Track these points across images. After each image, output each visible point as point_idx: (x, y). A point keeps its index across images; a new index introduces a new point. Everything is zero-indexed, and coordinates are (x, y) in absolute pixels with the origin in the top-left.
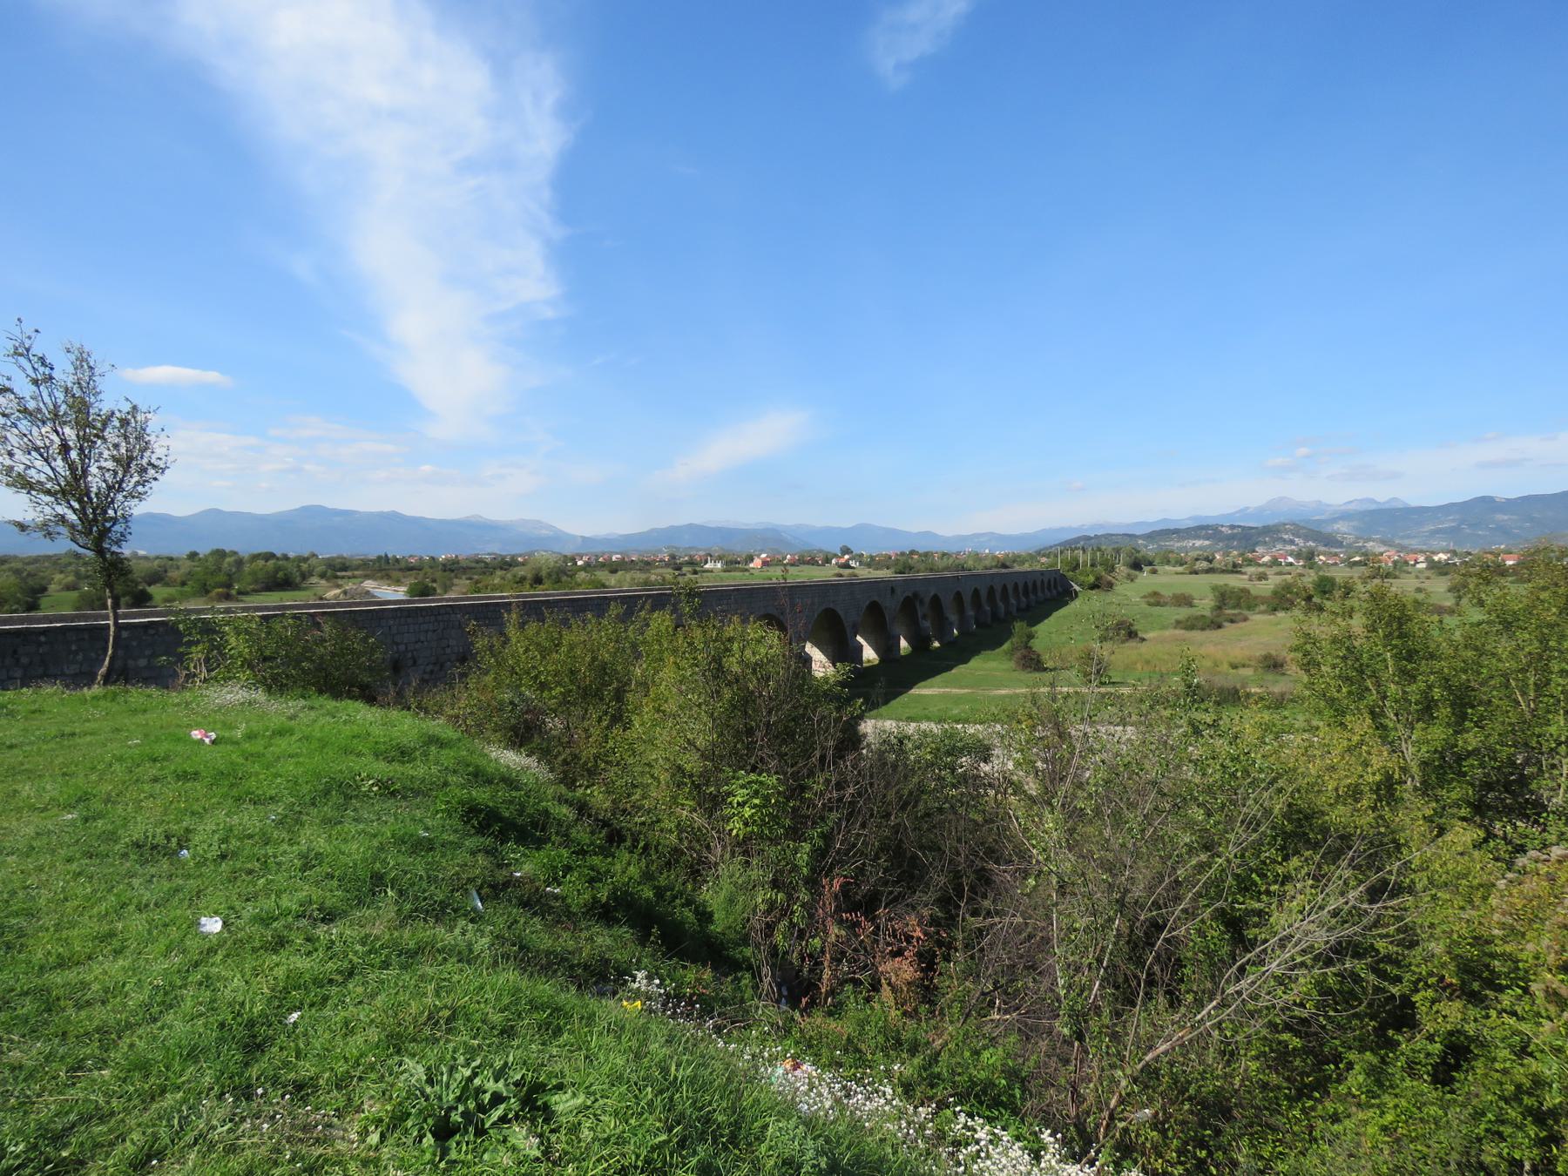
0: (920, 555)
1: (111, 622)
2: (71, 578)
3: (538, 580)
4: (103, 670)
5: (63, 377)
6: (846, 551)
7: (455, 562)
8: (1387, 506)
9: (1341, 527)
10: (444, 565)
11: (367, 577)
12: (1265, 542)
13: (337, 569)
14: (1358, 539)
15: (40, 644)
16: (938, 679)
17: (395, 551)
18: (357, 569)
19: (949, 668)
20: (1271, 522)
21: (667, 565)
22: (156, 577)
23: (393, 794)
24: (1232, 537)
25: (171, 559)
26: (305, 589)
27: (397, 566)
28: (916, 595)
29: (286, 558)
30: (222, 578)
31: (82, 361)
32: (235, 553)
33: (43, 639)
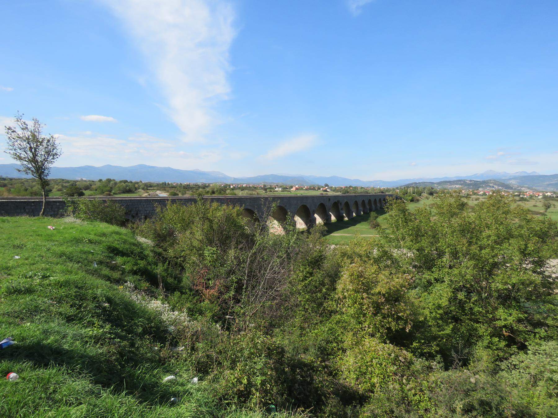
0: (353, 188)
1: (44, 200)
2: (60, 187)
3: (213, 192)
4: (41, 213)
5: (31, 127)
6: (327, 185)
7: (188, 185)
8: (532, 174)
9: (513, 182)
10: (184, 186)
11: (158, 190)
12: (483, 187)
13: (148, 187)
14: (518, 187)
15: (32, 206)
16: (342, 231)
17: (169, 181)
18: (155, 187)
19: (348, 227)
20: (486, 179)
21: (262, 189)
22: (87, 188)
23: (91, 243)
24: (470, 185)
25: (93, 182)
26: (136, 193)
27: (169, 186)
28: (338, 201)
29: (131, 182)
30: (108, 188)
31: (36, 122)
32: (114, 180)
33: (33, 204)
